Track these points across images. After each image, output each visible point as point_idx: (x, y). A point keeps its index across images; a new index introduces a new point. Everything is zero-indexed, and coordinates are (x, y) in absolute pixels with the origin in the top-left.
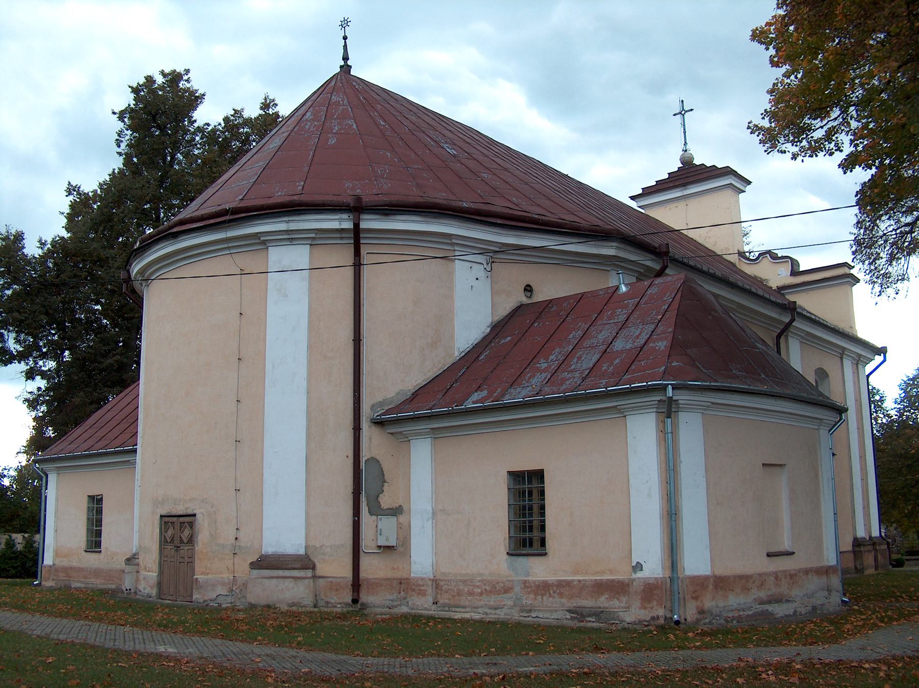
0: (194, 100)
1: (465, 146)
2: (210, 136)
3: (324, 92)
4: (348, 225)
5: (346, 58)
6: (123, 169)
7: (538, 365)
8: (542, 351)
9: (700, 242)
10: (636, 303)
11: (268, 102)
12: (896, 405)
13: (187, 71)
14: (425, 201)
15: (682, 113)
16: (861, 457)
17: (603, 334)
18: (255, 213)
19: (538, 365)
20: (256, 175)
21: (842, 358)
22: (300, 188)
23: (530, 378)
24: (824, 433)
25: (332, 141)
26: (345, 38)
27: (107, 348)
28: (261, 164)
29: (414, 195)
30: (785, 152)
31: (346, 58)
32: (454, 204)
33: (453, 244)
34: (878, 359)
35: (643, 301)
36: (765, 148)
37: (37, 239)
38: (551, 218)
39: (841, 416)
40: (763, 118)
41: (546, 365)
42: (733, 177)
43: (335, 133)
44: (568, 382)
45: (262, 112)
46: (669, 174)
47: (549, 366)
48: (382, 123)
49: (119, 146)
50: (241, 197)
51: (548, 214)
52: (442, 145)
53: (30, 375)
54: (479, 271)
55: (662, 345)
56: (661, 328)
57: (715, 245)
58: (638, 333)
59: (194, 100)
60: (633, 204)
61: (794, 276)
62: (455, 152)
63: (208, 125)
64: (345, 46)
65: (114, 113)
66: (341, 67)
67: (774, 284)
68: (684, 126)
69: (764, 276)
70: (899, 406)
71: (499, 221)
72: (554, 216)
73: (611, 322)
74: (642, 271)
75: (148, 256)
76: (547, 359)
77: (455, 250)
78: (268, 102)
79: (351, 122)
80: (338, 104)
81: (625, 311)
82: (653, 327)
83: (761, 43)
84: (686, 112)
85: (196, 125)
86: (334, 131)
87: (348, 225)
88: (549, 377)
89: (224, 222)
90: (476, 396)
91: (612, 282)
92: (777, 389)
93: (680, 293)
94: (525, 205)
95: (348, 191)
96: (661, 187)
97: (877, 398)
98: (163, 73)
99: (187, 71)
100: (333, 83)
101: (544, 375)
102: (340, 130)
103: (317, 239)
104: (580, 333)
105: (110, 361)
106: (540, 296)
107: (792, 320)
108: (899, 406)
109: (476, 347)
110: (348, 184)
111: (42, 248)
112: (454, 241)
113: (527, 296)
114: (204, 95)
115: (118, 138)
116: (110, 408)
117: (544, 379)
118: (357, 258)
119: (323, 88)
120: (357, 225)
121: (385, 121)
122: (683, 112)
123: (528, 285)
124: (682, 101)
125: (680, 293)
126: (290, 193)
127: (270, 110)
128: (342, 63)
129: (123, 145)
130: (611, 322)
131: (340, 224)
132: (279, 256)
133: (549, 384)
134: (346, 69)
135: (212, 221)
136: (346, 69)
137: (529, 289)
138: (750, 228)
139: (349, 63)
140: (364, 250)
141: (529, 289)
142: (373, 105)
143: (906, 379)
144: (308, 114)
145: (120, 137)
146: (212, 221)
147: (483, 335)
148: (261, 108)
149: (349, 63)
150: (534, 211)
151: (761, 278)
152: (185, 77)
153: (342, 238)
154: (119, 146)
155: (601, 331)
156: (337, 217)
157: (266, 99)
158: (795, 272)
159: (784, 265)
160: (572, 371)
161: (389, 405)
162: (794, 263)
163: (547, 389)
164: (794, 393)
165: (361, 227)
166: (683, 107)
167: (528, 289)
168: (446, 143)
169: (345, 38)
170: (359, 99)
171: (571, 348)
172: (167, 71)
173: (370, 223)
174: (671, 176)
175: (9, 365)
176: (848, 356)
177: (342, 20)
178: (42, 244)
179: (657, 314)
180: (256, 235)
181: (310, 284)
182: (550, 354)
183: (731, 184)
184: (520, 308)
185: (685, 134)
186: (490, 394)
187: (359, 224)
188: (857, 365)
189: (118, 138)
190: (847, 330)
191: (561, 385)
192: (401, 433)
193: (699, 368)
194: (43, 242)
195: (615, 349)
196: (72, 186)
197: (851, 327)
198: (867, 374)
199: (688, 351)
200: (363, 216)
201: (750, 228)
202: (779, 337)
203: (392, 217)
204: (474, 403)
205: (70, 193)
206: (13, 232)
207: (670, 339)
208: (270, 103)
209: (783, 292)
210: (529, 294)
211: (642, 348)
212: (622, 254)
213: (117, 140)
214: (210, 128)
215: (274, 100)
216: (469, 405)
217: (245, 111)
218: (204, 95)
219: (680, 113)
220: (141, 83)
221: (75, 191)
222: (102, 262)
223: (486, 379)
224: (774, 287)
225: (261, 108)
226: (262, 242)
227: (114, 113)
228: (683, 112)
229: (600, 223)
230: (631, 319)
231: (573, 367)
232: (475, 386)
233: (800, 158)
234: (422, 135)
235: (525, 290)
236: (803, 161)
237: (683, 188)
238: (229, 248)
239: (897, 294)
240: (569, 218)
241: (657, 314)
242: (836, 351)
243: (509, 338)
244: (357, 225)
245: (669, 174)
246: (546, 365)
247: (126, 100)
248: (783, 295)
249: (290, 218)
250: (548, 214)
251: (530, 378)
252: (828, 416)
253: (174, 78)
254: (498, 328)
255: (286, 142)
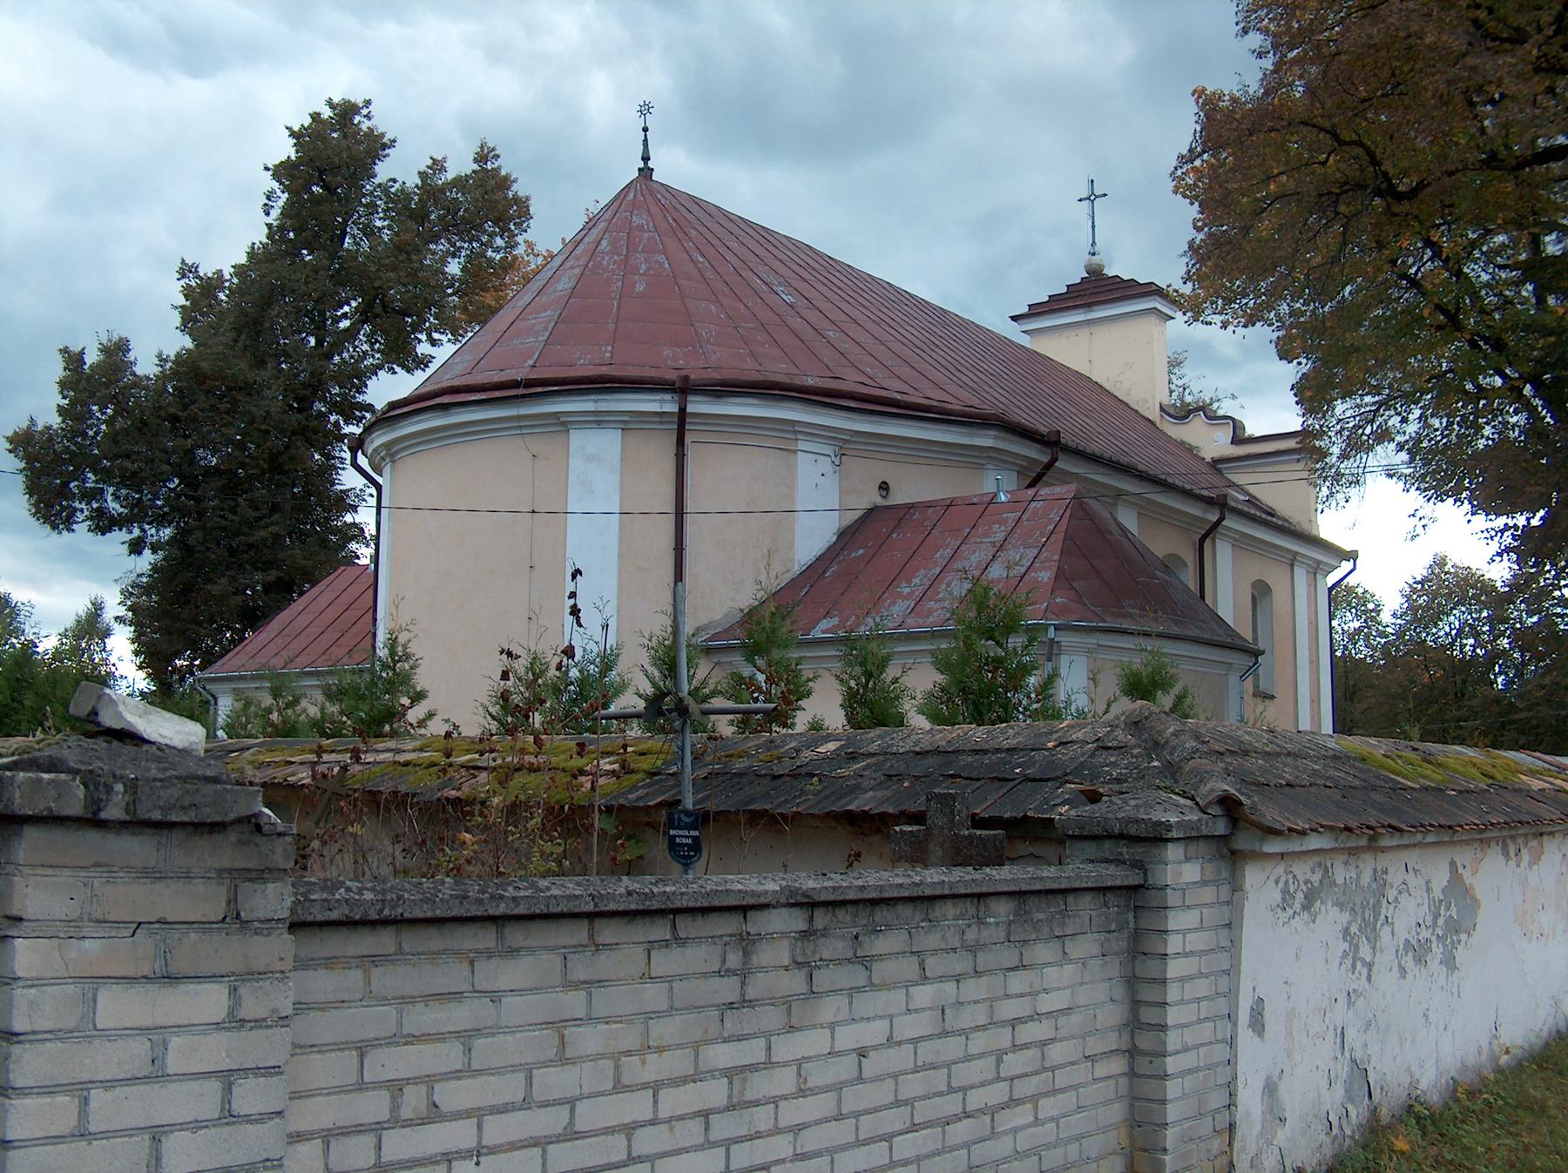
0: (377, 146)
1: (802, 286)
2: (398, 201)
3: (621, 209)
4: (672, 407)
5: (646, 159)
6: (267, 244)
7: (899, 590)
8: (903, 571)
9: (1108, 388)
10: (1017, 518)
11: (486, 151)
12: (1394, 620)
13: (368, 103)
14: (762, 378)
15: (1091, 198)
16: (1312, 701)
17: (975, 557)
18: (555, 388)
19: (899, 590)
20: (547, 330)
21: (1292, 566)
22: (608, 355)
23: (889, 606)
24: (1233, 679)
25: (640, 288)
26: (645, 130)
27: (257, 514)
28: (549, 313)
29: (748, 370)
30: (1211, 323)
31: (646, 159)
32: (797, 381)
33: (796, 432)
34: (1346, 566)
35: (1025, 517)
36: (1186, 318)
37: (156, 352)
38: (915, 399)
39: (1257, 659)
40: (1185, 283)
41: (908, 590)
42: (1158, 298)
43: (642, 275)
44: (935, 614)
45: (476, 167)
46: (1068, 286)
47: (912, 593)
48: (701, 259)
49: (268, 214)
50: (531, 362)
51: (911, 391)
52: (775, 288)
53: (136, 547)
54: (825, 465)
55: (1045, 576)
56: (1044, 554)
57: (1128, 394)
58: (1019, 555)
59: (377, 146)
60: (1014, 332)
61: (1236, 444)
62: (792, 300)
63: (395, 181)
64: (646, 141)
65: (267, 169)
66: (640, 170)
67: (1208, 453)
68: (1093, 217)
69: (1194, 443)
70: (1399, 621)
71: (853, 404)
72: (918, 394)
73: (987, 540)
74: (1025, 464)
75: (404, 427)
76: (909, 582)
77: (797, 439)
78: (486, 151)
79: (661, 258)
80: (641, 228)
81: (1003, 528)
82: (1036, 551)
83: (1185, 196)
84: (1097, 197)
85: (377, 181)
86: (641, 271)
87: (672, 407)
88: (913, 605)
89: (516, 397)
90: (825, 624)
91: (989, 487)
92: (1176, 630)
93: (1069, 510)
94: (882, 378)
95: (669, 362)
96: (1055, 305)
97: (1371, 606)
98: (330, 103)
99: (368, 103)
100: (631, 196)
101: (907, 603)
102: (649, 269)
103: (629, 423)
104: (949, 552)
105: (263, 533)
106: (898, 497)
107: (1222, 519)
108: (1399, 621)
109: (819, 559)
110: (666, 352)
111: (161, 366)
112: (797, 428)
113: (881, 496)
114: (394, 141)
115: (267, 202)
116: (300, 608)
117: (908, 608)
118: (680, 449)
119: (618, 202)
120: (683, 410)
121: (703, 256)
122: (1092, 198)
123: (884, 483)
124: (1092, 181)
125: (1069, 510)
126: (596, 362)
127: (489, 163)
128: (641, 165)
129: (275, 213)
130: (987, 540)
131: (661, 407)
132: (580, 440)
133: (912, 615)
134: (646, 172)
135: (497, 394)
136: (646, 172)
137: (884, 486)
138: (1185, 355)
139: (650, 164)
140: (688, 439)
141: (884, 486)
142: (686, 230)
143: (1411, 581)
144: (604, 243)
145: (270, 200)
146: (497, 394)
147: (829, 544)
148: (475, 161)
149: (650, 164)
150: (894, 388)
151: (1190, 445)
152: (365, 112)
153: (661, 423)
154: (268, 214)
155: (974, 552)
156: (659, 397)
157: (482, 147)
158: (1239, 438)
159: (1225, 427)
160: (940, 600)
161: (715, 628)
162: (1237, 426)
163: (910, 621)
164: (1194, 633)
165: (688, 410)
166: (1092, 189)
167: (884, 487)
168: (780, 284)
169: (645, 130)
170: (668, 220)
171: (939, 570)
172: (336, 100)
173: (697, 405)
174: (1072, 289)
175: (108, 534)
176: (1303, 563)
177: (642, 104)
178: (162, 360)
179: (1041, 536)
180: (556, 415)
181: (622, 478)
182: (914, 577)
183: (1155, 308)
184: (872, 511)
185: (1093, 229)
186: (843, 621)
187: (685, 409)
188: (1315, 574)
189: (267, 202)
190: (1305, 527)
191: (928, 616)
192: (731, 662)
193: (1085, 604)
194: (164, 357)
195: (991, 576)
196: (186, 265)
197: (1310, 521)
198: (1329, 585)
199: (1075, 584)
200: (690, 398)
201: (1185, 355)
202: (1202, 540)
203: (725, 400)
204: (823, 632)
205: (184, 276)
206: (115, 338)
207: (1055, 569)
208: (488, 152)
209: (1219, 466)
210: (884, 493)
211: (1022, 577)
212: (1001, 445)
213: (266, 205)
214: (397, 186)
215: (493, 150)
216: (817, 633)
217: (448, 161)
218: (394, 141)
219: (1089, 198)
220: (306, 125)
221: (191, 272)
222: (248, 388)
223: (836, 602)
224: (1208, 459)
225: (475, 161)
226: (563, 424)
227: (267, 169)
228: (1092, 198)
229: (976, 402)
230: (1012, 540)
231: (940, 596)
232: (822, 611)
233: (1231, 328)
234: (750, 274)
235: (880, 487)
236: (1234, 332)
237: (1086, 309)
238: (520, 427)
239: (1347, 501)
240: (937, 394)
241: (1041, 536)
242: (1284, 557)
243: (861, 551)
244: (683, 410)
245: (1068, 286)
246: (908, 590)
247: (286, 150)
248: (1219, 471)
249: (600, 397)
250: (911, 391)
251: (889, 606)
252: (1242, 661)
253: (346, 112)
254: (847, 536)
255: (580, 284)
